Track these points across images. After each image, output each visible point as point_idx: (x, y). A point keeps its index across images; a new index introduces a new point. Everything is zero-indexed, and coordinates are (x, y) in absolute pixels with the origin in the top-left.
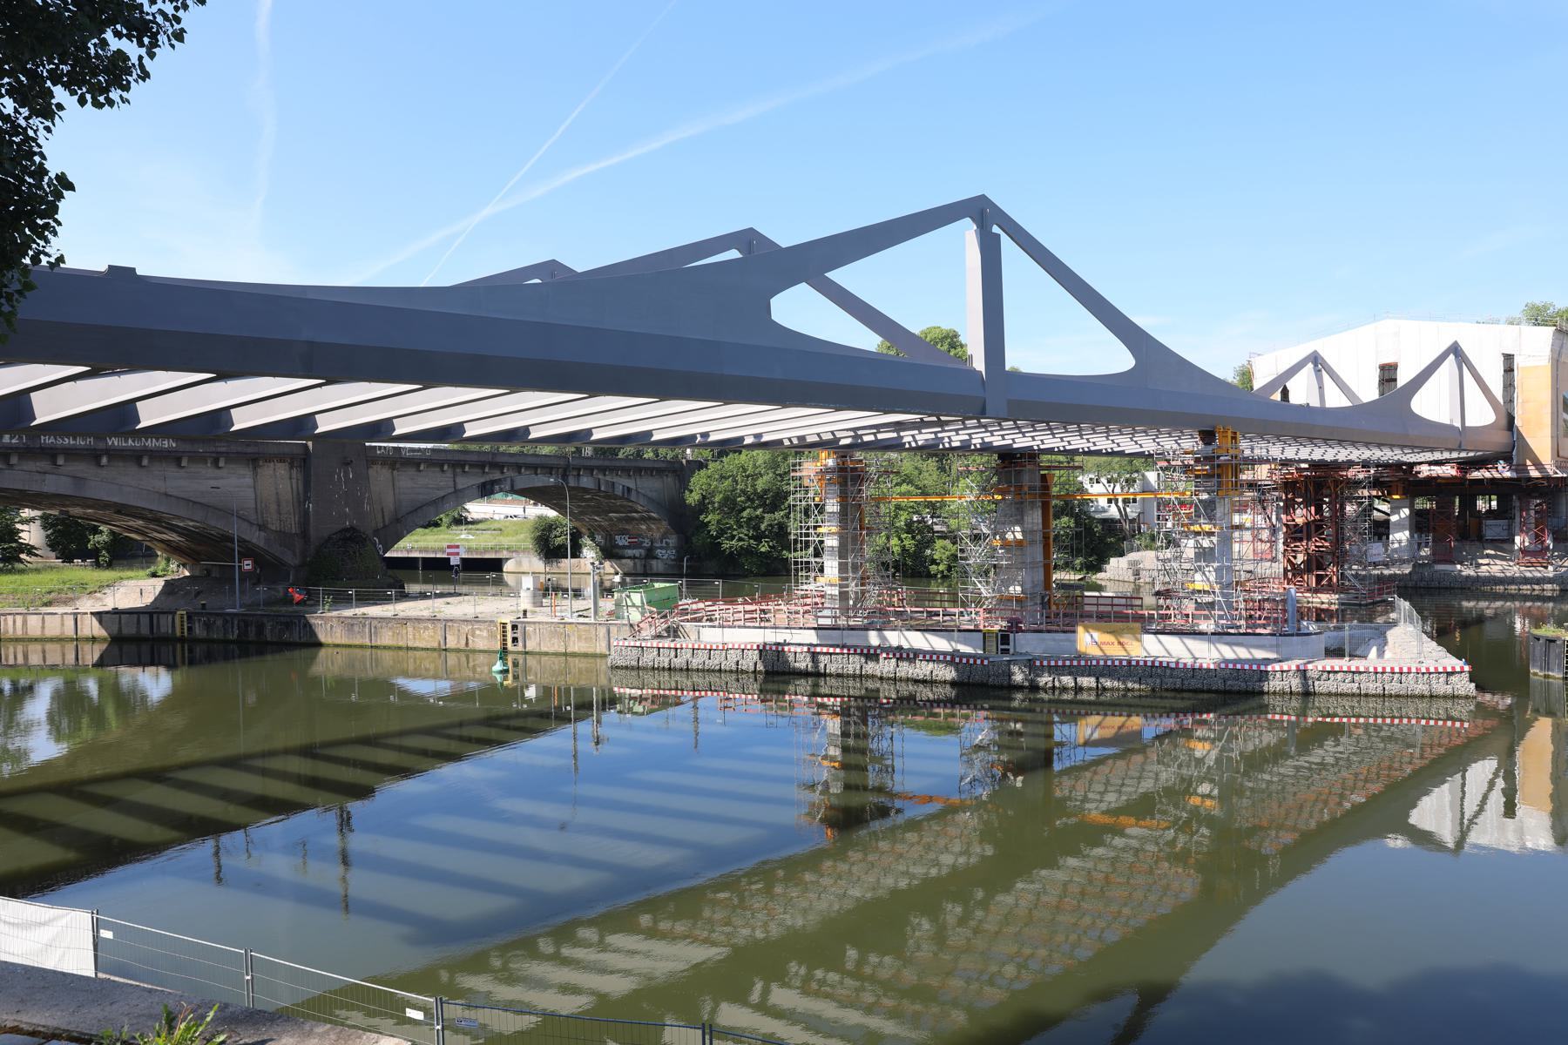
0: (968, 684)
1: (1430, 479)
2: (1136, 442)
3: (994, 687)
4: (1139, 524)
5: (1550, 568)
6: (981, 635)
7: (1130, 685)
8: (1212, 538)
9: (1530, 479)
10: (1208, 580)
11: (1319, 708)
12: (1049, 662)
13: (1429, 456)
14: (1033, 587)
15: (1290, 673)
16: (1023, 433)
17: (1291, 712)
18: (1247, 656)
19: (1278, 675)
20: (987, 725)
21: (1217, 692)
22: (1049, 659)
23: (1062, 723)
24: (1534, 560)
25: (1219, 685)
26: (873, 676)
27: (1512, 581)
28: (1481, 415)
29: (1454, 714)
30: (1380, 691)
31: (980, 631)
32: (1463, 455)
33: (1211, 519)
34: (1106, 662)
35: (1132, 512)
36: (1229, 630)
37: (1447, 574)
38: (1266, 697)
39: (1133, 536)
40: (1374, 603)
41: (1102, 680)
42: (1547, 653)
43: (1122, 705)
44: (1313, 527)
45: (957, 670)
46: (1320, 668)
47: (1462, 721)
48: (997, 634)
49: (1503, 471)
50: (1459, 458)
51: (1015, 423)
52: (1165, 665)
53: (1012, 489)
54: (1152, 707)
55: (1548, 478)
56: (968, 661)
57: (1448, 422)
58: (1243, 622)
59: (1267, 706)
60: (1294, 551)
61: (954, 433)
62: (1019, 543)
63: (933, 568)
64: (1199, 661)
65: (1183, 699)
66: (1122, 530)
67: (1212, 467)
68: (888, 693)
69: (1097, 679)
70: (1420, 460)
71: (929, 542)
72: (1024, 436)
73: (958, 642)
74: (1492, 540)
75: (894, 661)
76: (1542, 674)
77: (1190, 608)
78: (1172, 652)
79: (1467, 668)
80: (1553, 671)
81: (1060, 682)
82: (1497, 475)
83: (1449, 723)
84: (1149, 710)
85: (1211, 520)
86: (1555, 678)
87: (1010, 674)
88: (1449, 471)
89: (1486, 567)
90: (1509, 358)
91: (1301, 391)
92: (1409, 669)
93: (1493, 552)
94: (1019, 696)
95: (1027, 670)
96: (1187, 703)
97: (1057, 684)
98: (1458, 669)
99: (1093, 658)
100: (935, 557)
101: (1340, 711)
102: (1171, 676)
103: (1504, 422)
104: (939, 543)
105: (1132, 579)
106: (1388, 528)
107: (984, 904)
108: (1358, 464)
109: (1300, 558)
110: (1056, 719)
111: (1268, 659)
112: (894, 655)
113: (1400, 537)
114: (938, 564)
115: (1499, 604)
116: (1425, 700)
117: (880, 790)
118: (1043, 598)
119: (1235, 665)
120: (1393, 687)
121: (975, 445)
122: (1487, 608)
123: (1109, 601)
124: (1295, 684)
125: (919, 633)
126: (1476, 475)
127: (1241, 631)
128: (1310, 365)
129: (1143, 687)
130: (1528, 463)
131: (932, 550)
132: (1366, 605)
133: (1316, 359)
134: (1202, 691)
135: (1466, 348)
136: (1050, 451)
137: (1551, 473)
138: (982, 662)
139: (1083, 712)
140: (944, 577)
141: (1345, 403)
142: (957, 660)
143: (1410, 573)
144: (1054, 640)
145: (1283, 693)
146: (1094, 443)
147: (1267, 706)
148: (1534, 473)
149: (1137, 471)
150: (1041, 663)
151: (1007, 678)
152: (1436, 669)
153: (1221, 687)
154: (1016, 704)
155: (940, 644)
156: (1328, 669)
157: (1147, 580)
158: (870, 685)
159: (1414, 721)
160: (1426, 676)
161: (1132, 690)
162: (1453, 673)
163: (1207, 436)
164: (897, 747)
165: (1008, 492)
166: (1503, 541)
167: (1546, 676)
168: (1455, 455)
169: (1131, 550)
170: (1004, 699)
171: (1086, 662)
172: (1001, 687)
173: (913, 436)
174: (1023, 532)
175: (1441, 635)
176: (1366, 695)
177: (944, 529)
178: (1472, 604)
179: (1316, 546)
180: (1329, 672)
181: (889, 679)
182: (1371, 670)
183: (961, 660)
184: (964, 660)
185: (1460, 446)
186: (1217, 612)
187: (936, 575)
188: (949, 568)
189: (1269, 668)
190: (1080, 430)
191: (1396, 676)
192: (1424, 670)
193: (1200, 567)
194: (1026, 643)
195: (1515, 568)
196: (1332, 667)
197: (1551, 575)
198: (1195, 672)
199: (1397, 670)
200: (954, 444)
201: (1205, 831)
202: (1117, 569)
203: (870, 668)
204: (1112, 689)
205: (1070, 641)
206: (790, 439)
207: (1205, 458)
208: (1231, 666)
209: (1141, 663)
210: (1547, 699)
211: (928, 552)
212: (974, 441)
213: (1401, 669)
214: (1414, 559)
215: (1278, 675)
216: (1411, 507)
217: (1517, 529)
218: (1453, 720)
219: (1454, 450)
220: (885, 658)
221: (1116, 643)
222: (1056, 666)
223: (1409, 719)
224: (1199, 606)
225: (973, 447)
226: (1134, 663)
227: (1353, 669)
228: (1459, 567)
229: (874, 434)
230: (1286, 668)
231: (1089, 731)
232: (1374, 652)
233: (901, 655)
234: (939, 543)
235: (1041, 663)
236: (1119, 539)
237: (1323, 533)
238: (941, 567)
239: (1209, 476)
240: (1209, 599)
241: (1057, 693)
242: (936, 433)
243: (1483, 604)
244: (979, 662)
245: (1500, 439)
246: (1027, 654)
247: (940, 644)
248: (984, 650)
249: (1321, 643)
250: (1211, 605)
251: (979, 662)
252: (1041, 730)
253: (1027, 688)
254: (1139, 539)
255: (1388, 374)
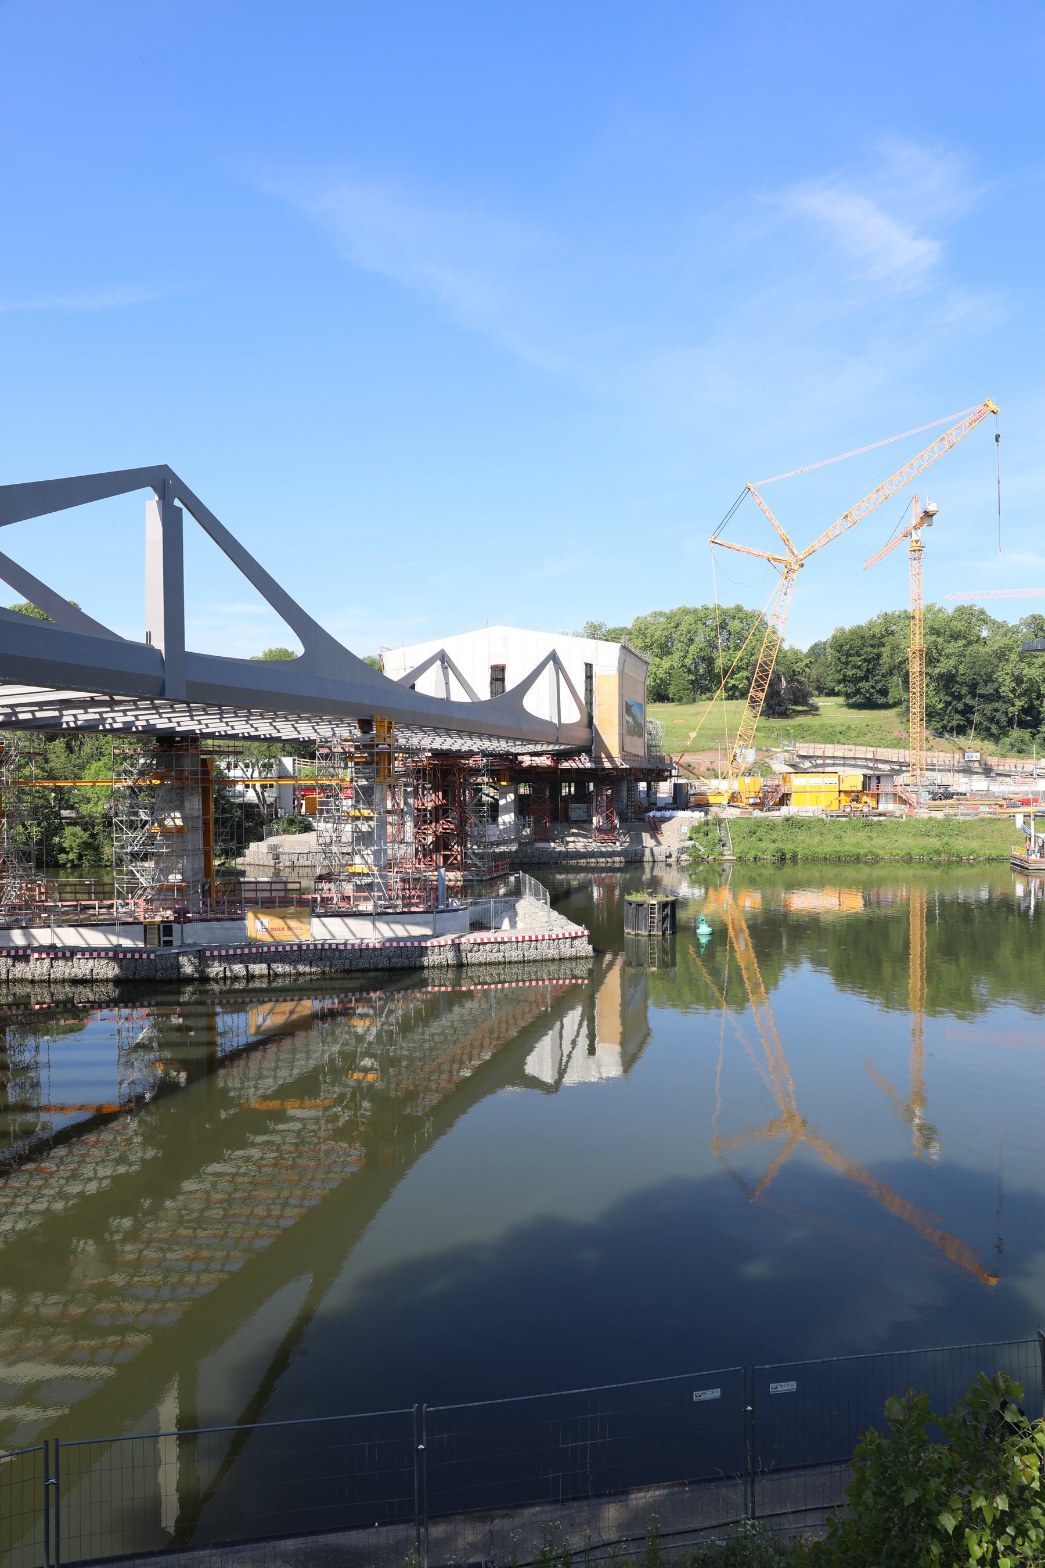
0: (134, 981)
1: (531, 768)
2: (251, 725)
3: (163, 982)
4: (276, 808)
5: (618, 844)
6: (142, 927)
7: (301, 968)
8: (371, 823)
9: (604, 769)
10: (367, 862)
11: (471, 978)
12: (220, 952)
13: (532, 748)
14: (193, 875)
15: (447, 948)
16: (160, 714)
17: (447, 983)
18: (404, 934)
19: (436, 950)
20: (147, 1023)
21: (382, 970)
22: (219, 948)
23: (224, 1013)
24: (606, 837)
25: (384, 963)
26: (22, 981)
27: (592, 854)
28: (572, 715)
29: (577, 972)
30: (520, 958)
31: (141, 923)
32: (557, 747)
33: (369, 804)
34: (277, 948)
35: (270, 796)
36: (387, 910)
37: (545, 850)
38: (426, 972)
39: (271, 821)
40: (492, 879)
41: (274, 966)
42: (637, 916)
43: (296, 990)
44: (441, 812)
45: (121, 967)
46: (472, 941)
47: (583, 978)
48: (159, 926)
49: (584, 762)
50: (552, 750)
51: (152, 703)
52: (334, 947)
53: (173, 774)
54: (322, 989)
55: (616, 769)
56: (133, 956)
57: (548, 719)
58: (399, 902)
59: (427, 979)
60: (424, 833)
61: (121, 714)
62: (179, 830)
63: (62, 858)
64: (365, 941)
65: (351, 979)
66: (259, 814)
67: (371, 755)
68: (40, 999)
69: (269, 965)
70: (524, 751)
71: (56, 829)
72: (161, 717)
73: (119, 935)
74: (576, 821)
75: (47, 961)
76: (633, 933)
77: (348, 888)
78: (335, 935)
79: (586, 933)
80: (641, 930)
81: (231, 971)
82: (581, 766)
83: (574, 981)
84: (320, 992)
85: (369, 805)
86: (643, 936)
87: (179, 967)
88: (545, 761)
89: (572, 844)
90: (589, 667)
91: (428, 685)
92: (543, 936)
93: (576, 831)
94: (190, 989)
95: (196, 961)
96: (356, 984)
97: (228, 974)
98: (580, 934)
99: (264, 944)
100: (64, 845)
101: (488, 979)
102: (340, 958)
103: (586, 721)
104: (69, 830)
105: (272, 863)
106: (497, 811)
107: (154, 1212)
108: (477, 754)
109: (430, 839)
110: (219, 1009)
111: (426, 936)
112: (48, 954)
113: (507, 818)
114: (67, 853)
115: (582, 875)
116: (556, 963)
117: (24, 1108)
118: (203, 886)
119: (398, 943)
120: (531, 954)
121: (67, 723)
122: (573, 880)
123: (267, 887)
124: (450, 956)
125: (72, 929)
126: (566, 765)
127: (398, 910)
128: (438, 663)
129: (314, 969)
130: (603, 756)
131: (61, 837)
132: (487, 880)
133: (442, 657)
134: (370, 970)
135: (560, 655)
136: (211, 736)
137: (619, 764)
138: (149, 956)
139: (247, 1000)
140: (74, 866)
141: (466, 699)
142: (121, 956)
143: (517, 851)
144: (225, 929)
145: (440, 967)
146: (232, 727)
147: (427, 979)
148: (607, 765)
149: (275, 757)
150: (212, 953)
151: (176, 971)
152: (564, 935)
153: (387, 965)
154: (185, 998)
155: (96, 938)
156: (479, 941)
157: (288, 863)
158: (19, 990)
159: (547, 982)
160: (556, 942)
161: (304, 974)
162: (573, 938)
163: (365, 725)
164: (42, 1057)
165: (168, 777)
166: (584, 822)
167: (637, 935)
168: (551, 747)
169: (270, 834)
170: (173, 993)
171: (257, 949)
172: (170, 981)
173: (75, 716)
174: (183, 818)
175: (556, 903)
176: (510, 963)
177: (73, 815)
178: (563, 877)
179: (443, 829)
180: (479, 944)
181: (42, 981)
182: (514, 939)
183: (125, 956)
184: (129, 956)
185: (557, 740)
186: (376, 894)
187: (64, 865)
188: (80, 857)
189: (429, 944)
190: (190, 710)
191: (533, 943)
192: (554, 937)
193: (359, 850)
194: (196, 933)
195: (594, 844)
196: (482, 939)
197: (619, 849)
198: (362, 951)
199: (533, 938)
200: (116, 726)
201: (366, 1104)
202: (257, 852)
203: (21, 970)
204: (284, 975)
205: (240, 929)
206: (219, 732)
207: (364, 746)
208: (395, 944)
209: (312, 947)
210: (637, 954)
211: (56, 840)
212: (65, 719)
213: (537, 937)
214: (518, 839)
215: (436, 950)
216: (516, 792)
217: (594, 811)
218: (576, 978)
219: (552, 743)
220: (37, 959)
221: (286, 928)
222: (227, 955)
223: (543, 980)
224: (359, 888)
225: (134, 729)
226: (304, 947)
227: (499, 940)
228: (552, 844)
229: (33, 712)
230: (443, 943)
231: (260, 1020)
232: (506, 924)
233: (56, 954)
234: (69, 830)
235: (212, 953)
236: (257, 824)
237: (448, 817)
238: (71, 856)
239: (367, 763)
240: (369, 880)
241: (228, 982)
242: (100, 713)
243: (571, 876)
244: (145, 956)
245: (583, 735)
246: (194, 944)
247: (96, 938)
248: (145, 943)
249: (465, 918)
250: (370, 886)
251: (145, 956)
252: (202, 1022)
253: (196, 979)
254: (277, 823)
255: (498, 674)
